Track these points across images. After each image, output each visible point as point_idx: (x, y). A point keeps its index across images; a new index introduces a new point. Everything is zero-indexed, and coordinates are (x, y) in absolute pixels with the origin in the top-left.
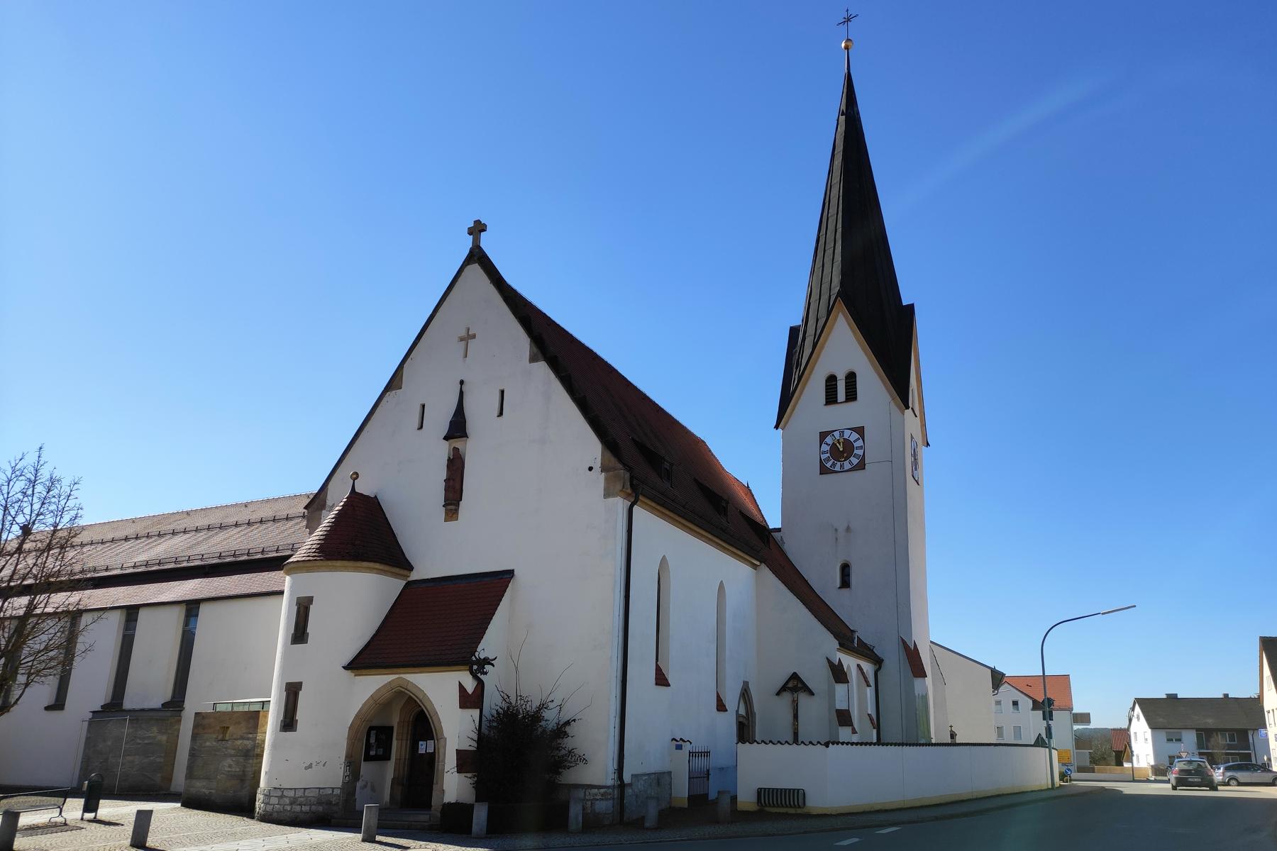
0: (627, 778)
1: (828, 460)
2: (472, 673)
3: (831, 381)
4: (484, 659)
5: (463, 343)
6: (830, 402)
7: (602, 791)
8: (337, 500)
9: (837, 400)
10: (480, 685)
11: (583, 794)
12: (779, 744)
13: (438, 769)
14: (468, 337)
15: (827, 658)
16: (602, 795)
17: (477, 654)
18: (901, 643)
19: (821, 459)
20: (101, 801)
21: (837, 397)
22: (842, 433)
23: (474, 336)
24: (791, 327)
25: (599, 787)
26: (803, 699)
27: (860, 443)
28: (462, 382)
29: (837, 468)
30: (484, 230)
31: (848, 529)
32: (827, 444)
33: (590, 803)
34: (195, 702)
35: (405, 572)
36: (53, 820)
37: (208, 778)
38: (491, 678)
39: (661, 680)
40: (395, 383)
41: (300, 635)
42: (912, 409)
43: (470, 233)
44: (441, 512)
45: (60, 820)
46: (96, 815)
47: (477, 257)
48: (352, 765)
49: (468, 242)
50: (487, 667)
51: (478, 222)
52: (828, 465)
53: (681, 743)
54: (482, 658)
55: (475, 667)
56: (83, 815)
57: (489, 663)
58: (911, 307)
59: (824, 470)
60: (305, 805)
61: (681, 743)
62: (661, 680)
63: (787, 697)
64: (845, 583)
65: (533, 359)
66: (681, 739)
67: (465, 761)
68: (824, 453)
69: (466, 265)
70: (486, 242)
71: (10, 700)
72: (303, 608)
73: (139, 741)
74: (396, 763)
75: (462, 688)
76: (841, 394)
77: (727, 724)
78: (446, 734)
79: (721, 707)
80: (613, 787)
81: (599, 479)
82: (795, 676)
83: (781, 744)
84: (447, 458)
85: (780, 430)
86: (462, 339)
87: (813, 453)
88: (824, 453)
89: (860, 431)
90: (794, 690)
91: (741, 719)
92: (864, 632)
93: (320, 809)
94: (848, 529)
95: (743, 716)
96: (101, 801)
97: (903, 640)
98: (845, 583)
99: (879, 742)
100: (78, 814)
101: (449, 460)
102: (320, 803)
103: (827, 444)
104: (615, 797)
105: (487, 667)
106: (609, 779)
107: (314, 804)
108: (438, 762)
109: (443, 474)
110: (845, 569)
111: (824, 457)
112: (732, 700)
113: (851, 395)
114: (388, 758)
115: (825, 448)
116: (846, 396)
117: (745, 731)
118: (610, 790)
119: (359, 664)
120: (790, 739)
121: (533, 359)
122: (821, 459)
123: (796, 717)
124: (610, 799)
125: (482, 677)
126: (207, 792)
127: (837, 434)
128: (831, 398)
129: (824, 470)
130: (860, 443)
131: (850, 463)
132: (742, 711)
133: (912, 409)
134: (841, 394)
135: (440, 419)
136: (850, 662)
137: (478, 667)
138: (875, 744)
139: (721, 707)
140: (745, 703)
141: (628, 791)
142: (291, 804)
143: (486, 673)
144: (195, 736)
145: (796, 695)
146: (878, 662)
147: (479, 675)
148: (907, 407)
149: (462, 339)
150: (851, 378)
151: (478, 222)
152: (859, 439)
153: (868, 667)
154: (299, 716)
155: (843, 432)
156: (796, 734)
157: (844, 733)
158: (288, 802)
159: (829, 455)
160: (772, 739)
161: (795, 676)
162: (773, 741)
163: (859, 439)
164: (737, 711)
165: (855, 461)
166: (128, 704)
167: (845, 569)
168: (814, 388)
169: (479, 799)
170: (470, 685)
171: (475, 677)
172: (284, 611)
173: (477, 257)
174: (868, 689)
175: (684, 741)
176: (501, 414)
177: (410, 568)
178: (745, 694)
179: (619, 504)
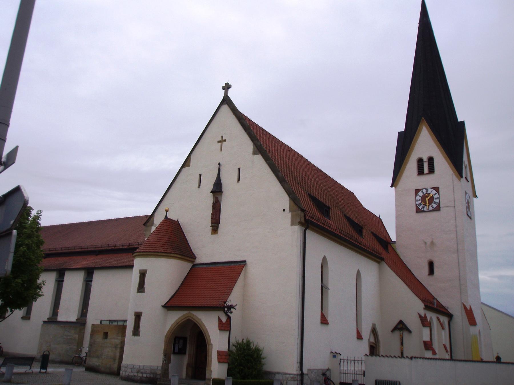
0: (305, 371)
1: (420, 204)
2: (224, 312)
3: (420, 161)
4: (231, 305)
5: (220, 144)
6: (420, 173)
7: (291, 376)
8: (158, 220)
9: (424, 173)
10: (229, 318)
11: (282, 377)
12: (386, 357)
13: (208, 360)
14: (222, 141)
15: (418, 313)
16: (291, 378)
17: (227, 303)
18: (463, 306)
19: (439, 195)
20: (459, 121)
21: (423, 171)
22: (427, 190)
23: (225, 141)
24: (399, 132)
25: (290, 374)
26: (405, 334)
27: (437, 196)
28: (219, 164)
29: (425, 209)
30: (230, 88)
31: (432, 243)
32: (419, 196)
33: (285, 381)
34: (92, 319)
35: (192, 260)
36: (27, 371)
37: (98, 357)
38: (234, 315)
39: (324, 321)
40: (186, 163)
41: (141, 288)
42: (466, 178)
43: (223, 89)
44: (210, 229)
45: (30, 371)
46: (46, 371)
47: (226, 101)
48: (167, 356)
49: (222, 93)
50: (232, 310)
51: (227, 84)
52: (420, 207)
53: (335, 354)
54: (230, 305)
55: (226, 309)
56: (40, 370)
57: (233, 308)
58: (463, 123)
59: (418, 211)
60: (144, 373)
61: (335, 354)
62: (324, 321)
63: (397, 333)
64: (431, 272)
65: (254, 153)
66: (335, 352)
67: (222, 357)
68: (418, 201)
69: (222, 105)
70: (231, 94)
71: (5, 314)
72: (143, 274)
73: (65, 337)
74: (188, 356)
75: (220, 320)
76: (426, 170)
77: (364, 347)
78: (212, 342)
79: (359, 337)
80: (298, 375)
81: (288, 215)
82: (401, 322)
83: (392, 357)
84: (212, 202)
85: (394, 188)
86: (219, 142)
87: (412, 201)
88: (418, 201)
89: (437, 189)
90: (401, 329)
91: (372, 344)
92: (444, 300)
93: (152, 376)
94: (432, 243)
95: (373, 343)
96: (459, 121)
97: (464, 305)
98: (431, 272)
99: (451, 359)
100: (38, 370)
101: (213, 203)
102: (151, 373)
103: (419, 196)
104: (299, 380)
105: (232, 310)
106: (293, 369)
107: (148, 374)
108: (209, 356)
109: (210, 211)
110: (431, 265)
111: (418, 203)
112: (366, 333)
113: (432, 170)
114: (185, 353)
115: (418, 198)
116: (429, 170)
117: (374, 350)
118: (296, 376)
119: (169, 306)
120: (400, 355)
121: (254, 153)
122: (439, 195)
123: (402, 344)
124: (296, 380)
125: (230, 314)
126: (98, 364)
127: (424, 191)
128: (421, 172)
129: (418, 211)
130: (437, 196)
131: (432, 206)
132: (372, 340)
133: (466, 178)
134: (426, 170)
135: (209, 184)
136: (431, 316)
137: (227, 309)
138: (448, 360)
139: (359, 337)
140: (374, 335)
141: (306, 378)
142: (137, 372)
143: (231, 313)
144: (92, 335)
145: (402, 332)
146: (450, 316)
147: (228, 313)
148: (462, 177)
149: (219, 142)
150: (431, 160)
151: (227, 84)
152: (436, 193)
153: (444, 320)
154: (141, 328)
155: (428, 190)
156: (402, 353)
157: (429, 354)
158: (136, 371)
159: (420, 202)
160: (395, 355)
161: (401, 322)
162: (383, 355)
163: (436, 193)
164: (369, 340)
165: (435, 206)
166: (60, 318)
167: (431, 265)
168: (411, 166)
169: (229, 375)
170: (224, 319)
171: (226, 314)
172: (135, 274)
173: (226, 101)
174: (443, 332)
175: (337, 353)
176: (239, 180)
177: (195, 258)
178: (374, 331)
179: (297, 229)
